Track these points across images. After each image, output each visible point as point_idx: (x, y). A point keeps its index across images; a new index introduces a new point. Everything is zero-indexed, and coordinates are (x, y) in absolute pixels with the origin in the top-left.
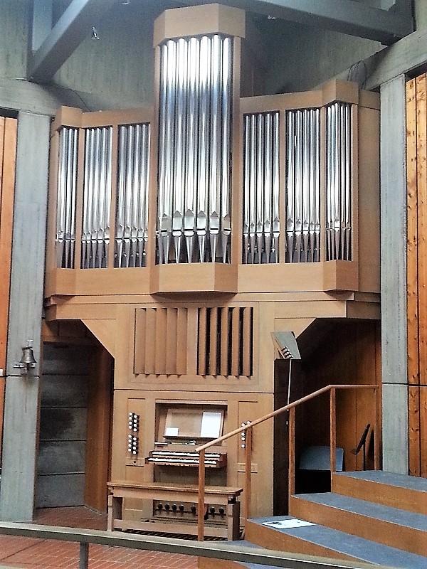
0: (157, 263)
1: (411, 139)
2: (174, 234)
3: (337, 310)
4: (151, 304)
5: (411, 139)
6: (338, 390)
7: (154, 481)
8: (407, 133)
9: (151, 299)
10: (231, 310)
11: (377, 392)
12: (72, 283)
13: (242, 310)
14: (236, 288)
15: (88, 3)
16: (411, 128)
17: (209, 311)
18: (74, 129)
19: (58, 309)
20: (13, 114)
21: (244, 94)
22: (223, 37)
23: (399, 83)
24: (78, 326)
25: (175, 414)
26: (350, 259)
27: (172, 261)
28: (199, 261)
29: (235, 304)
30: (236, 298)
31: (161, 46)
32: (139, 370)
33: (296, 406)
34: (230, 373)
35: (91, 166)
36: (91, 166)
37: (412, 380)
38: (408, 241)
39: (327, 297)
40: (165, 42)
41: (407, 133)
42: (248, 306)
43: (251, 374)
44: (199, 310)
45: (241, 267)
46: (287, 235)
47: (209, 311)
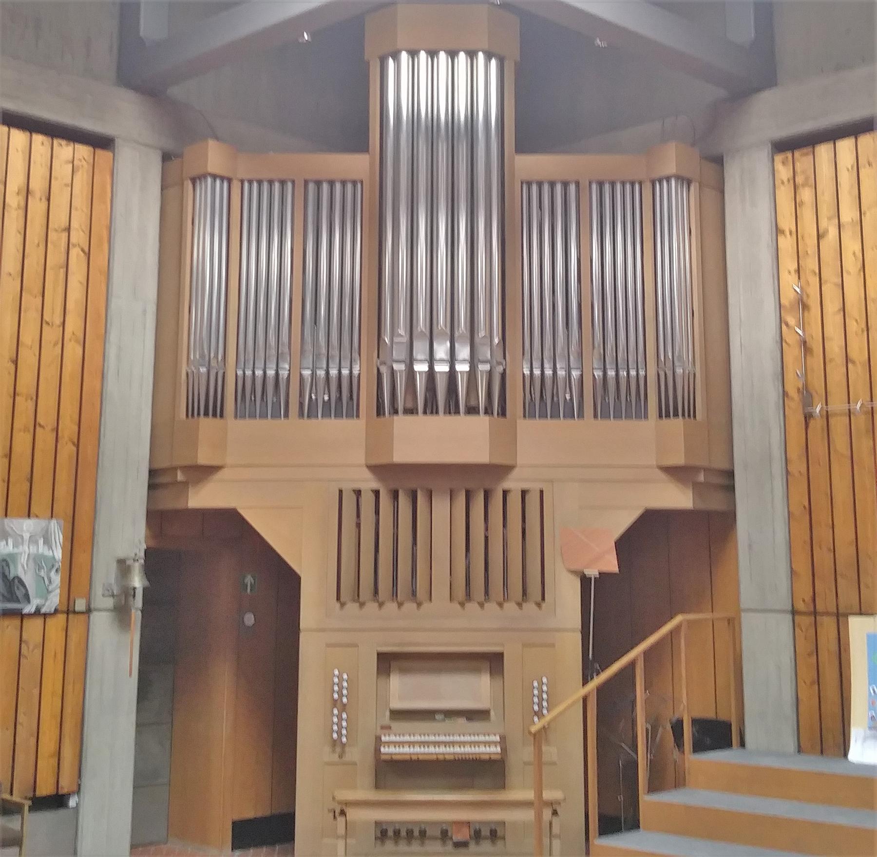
1: (786, 243)
2: (396, 367)
4: (368, 482)
5: (786, 243)
6: (689, 622)
8: (778, 231)
9: (367, 474)
10: (505, 493)
12: (406, 748)
13: (524, 493)
16: (786, 223)
17: (469, 495)
18: (222, 178)
19: (191, 491)
21: (521, 148)
22: (489, 56)
23: (764, 154)
25: (404, 671)
26: (695, 416)
27: (411, 411)
28: (457, 412)
29: (513, 483)
30: (515, 473)
31: (194, 181)
33: (647, 654)
34: (506, 598)
35: (648, 232)
36: (648, 232)
37: (801, 606)
38: (785, 394)
39: (662, 476)
40: (203, 177)
41: (778, 231)
42: (534, 487)
43: (543, 599)
44: (451, 492)
46: (594, 375)
47: (395, 495)
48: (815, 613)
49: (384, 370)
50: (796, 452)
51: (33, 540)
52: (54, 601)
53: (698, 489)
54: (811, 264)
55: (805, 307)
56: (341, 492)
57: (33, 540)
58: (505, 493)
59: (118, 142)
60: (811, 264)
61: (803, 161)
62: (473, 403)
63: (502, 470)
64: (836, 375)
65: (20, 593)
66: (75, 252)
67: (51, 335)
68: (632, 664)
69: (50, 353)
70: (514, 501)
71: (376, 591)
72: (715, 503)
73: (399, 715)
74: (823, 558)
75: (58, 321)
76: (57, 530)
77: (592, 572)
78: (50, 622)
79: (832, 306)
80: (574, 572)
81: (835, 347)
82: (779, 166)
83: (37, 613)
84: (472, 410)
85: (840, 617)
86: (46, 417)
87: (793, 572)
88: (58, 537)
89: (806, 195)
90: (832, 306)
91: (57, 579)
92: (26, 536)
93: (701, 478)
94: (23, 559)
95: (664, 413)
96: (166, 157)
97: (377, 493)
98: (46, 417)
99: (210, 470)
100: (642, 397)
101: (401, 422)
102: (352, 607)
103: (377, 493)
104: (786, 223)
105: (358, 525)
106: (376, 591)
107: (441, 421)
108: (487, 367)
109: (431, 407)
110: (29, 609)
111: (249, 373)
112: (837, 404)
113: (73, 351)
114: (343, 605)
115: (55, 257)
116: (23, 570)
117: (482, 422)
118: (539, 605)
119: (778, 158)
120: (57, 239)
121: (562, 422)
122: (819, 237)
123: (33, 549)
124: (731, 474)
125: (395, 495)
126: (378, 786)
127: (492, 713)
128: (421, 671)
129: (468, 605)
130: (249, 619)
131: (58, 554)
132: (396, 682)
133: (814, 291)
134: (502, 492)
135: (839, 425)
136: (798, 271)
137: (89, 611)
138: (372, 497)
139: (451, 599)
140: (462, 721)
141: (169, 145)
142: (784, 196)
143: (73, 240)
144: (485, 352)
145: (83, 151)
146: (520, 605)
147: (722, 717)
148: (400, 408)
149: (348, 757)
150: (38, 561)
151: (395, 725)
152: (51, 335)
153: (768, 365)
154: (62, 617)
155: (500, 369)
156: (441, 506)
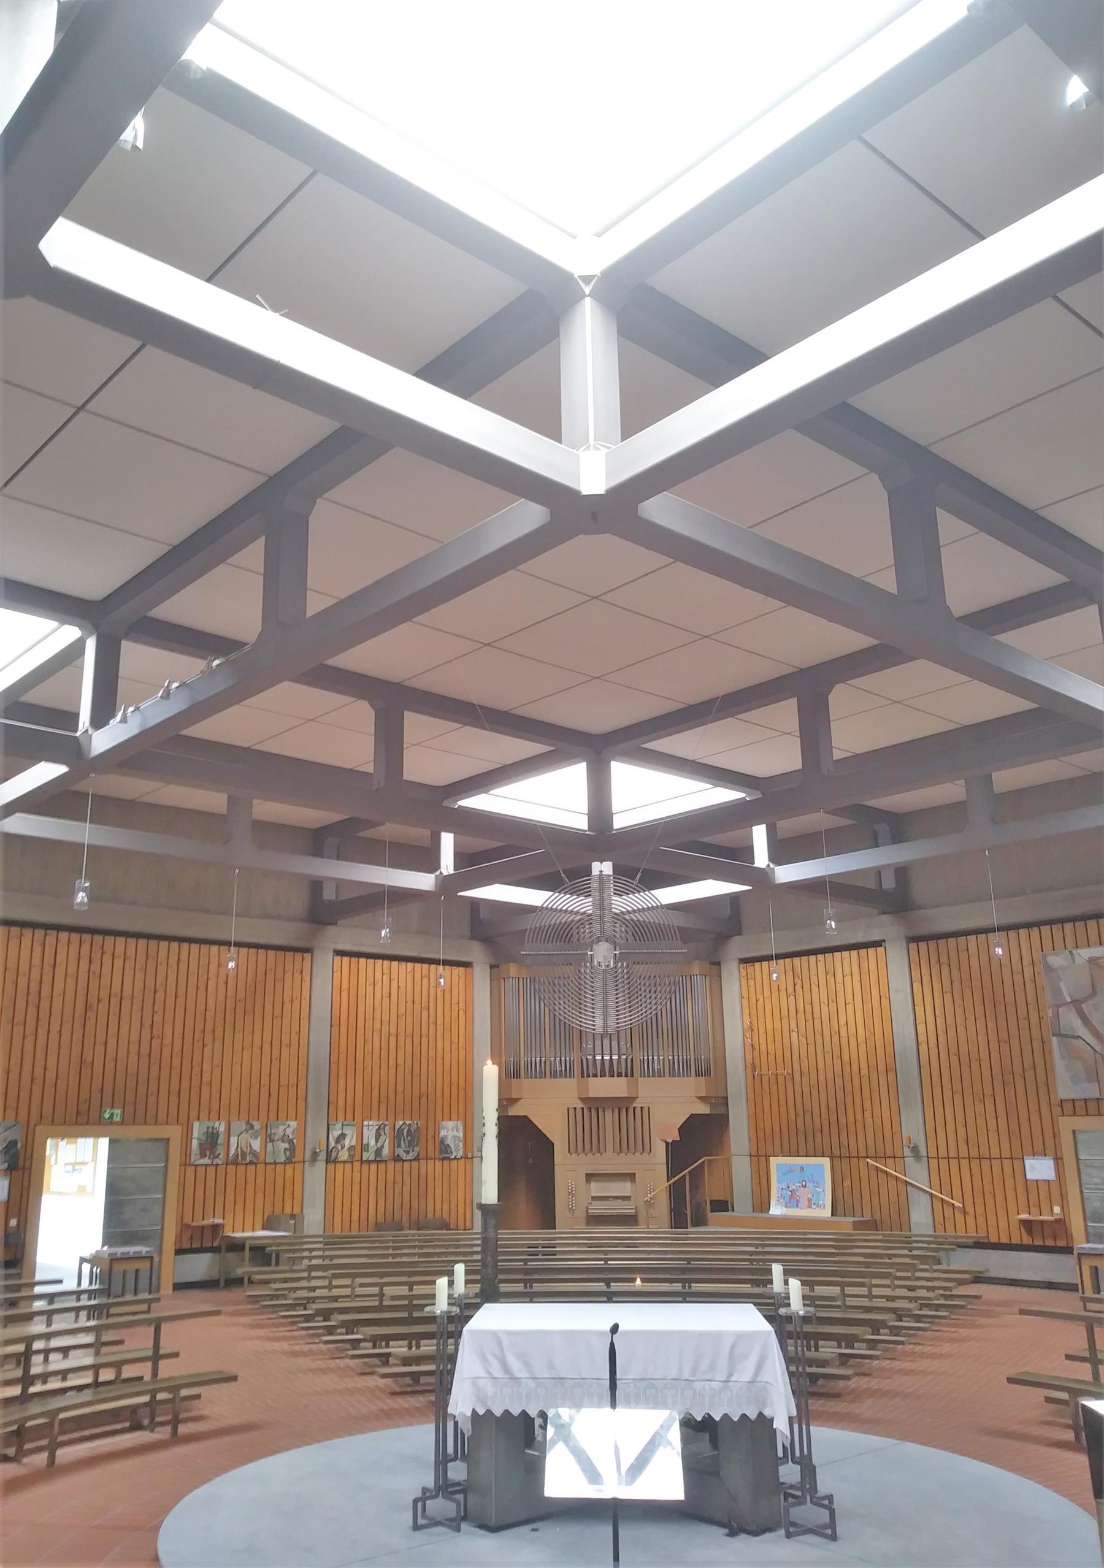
0: (583, 1076)
1: (745, 1002)
2: (588, 1057)
3: (703, 1109)
6: (708, 1160)
7: (754, 1211)
9: (579, 1101)
10: (634, 1108)
11: (728, 1161)
13: (642, 1108)
14: (638, 1094)
15: (1101, 712)
16: (745, 995)
20: (467, 965)
24: (525, 1119)
25: (596, 1181)
27: (595, 1075)
29: (637, 1104)
32: (572, 1149)
33: (689, 1172)
37: (753, 1153)
39: (697, 1100)
42: (645, 1105)
45: (640, 1079)
48: (969, 1158)
49: (584, 1058)
50: (750, 1090)
51: (452, 1130)
52: (460, 1154)
53: (712, 1105)
54: (754, 1012)
55: (752, 1030)
56: (1054, 950)
57: (453, 1130)
58: (634, 1108)
59: (474, 964)
60: (754, 1012)
61: (750, 969)
62: (620, 1071)
63: (632, 1099)
64: (764, 1059)
65: (449, 1151)
66: (461, 1012)
67: (454, 1046)
68: (685, 1175)
69: (455, 1054)
70: (638, 1111)
71: (584, 1150)
72: (720, 1110)
73: (594, 1198)
74: (761, 1134)
75: (457, 1041)
76: (460, 1124)
77: (670, 1140)
78: (460, 1161)
79: (762, 1031)
80: (662, 1140)
81: (763, 1047)
82: (742, 970)
83: (455, 1158)
84: (620, 1075)
85: (767, 1157)
86: (454, 1081)
87: (750, 1139)
88: (461, 1128)
89: (751, 982)
90: (762, 1031)
91: (461, 1144)
92: (450, 1128)
93: (713, 1101)
94: (450, 1137)
95: (698, 1074)
96: (492, 967)
97: (583, 1108)
98: (454, 1081)
99: (517, 1100)
100: (689, 1067)
101: (591, 1079)
102: (590, 1155)
103: (583, 1108)
104: (745, 995)
105: (576, 1122)
106: (584, 1150)
107: (607, 1080)
108: (625, 1057)
109: (603, 1075)
110: (452, 1157)
111: (529, 1059)
112: (764, 1071)
113: (462, 1053)
114: (571, 1155)
115: (455, 1014)
116: (449, 1141)
117: (624, 1079)
118: (649, 1154)
119: (741, 966)
120: (455, 1007)
121: (657, 1079)
122: (757, 1001)
123: (453, 1133)
124: (727, 1097)
125: (590, 1110)
126: (587, 1225)
127: (632, 1198)
128: (603, 1181)
129: (621, 1154)
130: (531, 1161)
131: (461, 1135)
132: (593, 1185)
133: (755, 1023)
134: (198, 1393)
135: (765, 1079)
136: (750, 1014)
137: (472, 1158)
138: (581, 1110)
139: (614, 1152)
140: (620, 1201)
141: (493, 962)
142: (744, 981)
143: (460, 1007)
144: (623, 1051)
145: (462, 969)
146: (641, 1154)
147: (727, 1200)
148: (591, 1075)
149: (575, 1215)
150: (455, 1137)
151: (593, 1202)
152: (454, 1046)
153: (740, 1053)
154: (463, 1160)
155: (630, 1057)
156: (609, 1114)
